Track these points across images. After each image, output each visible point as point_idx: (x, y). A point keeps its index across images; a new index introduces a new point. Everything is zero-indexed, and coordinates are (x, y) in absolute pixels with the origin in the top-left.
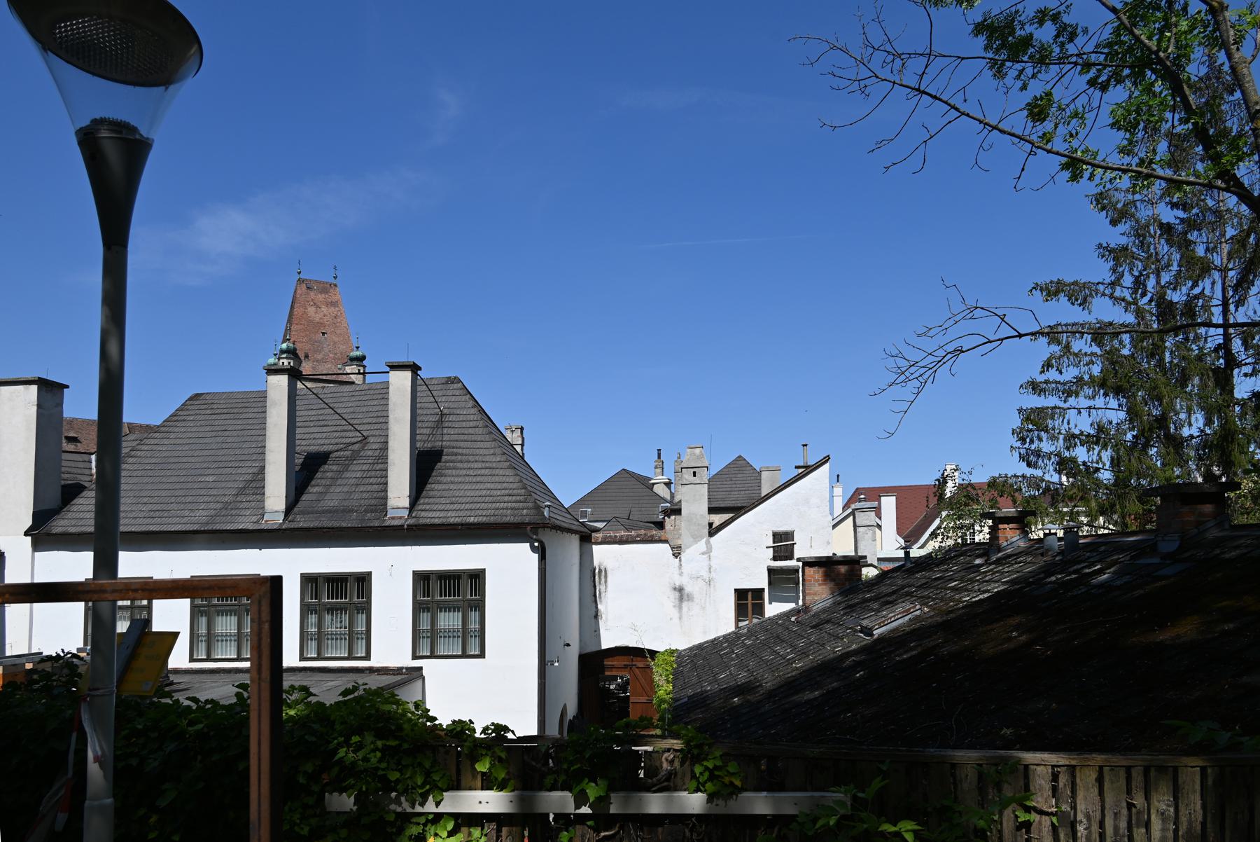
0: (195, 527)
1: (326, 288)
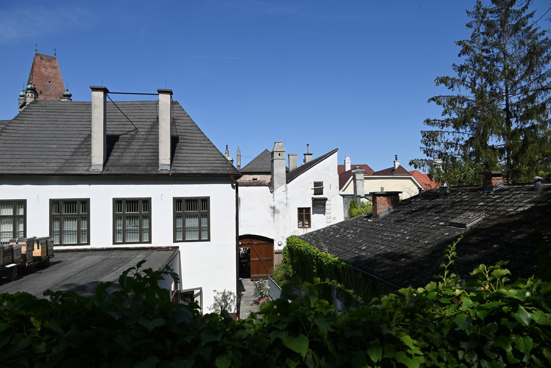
0: (53, 172)
1: (51, 59)
